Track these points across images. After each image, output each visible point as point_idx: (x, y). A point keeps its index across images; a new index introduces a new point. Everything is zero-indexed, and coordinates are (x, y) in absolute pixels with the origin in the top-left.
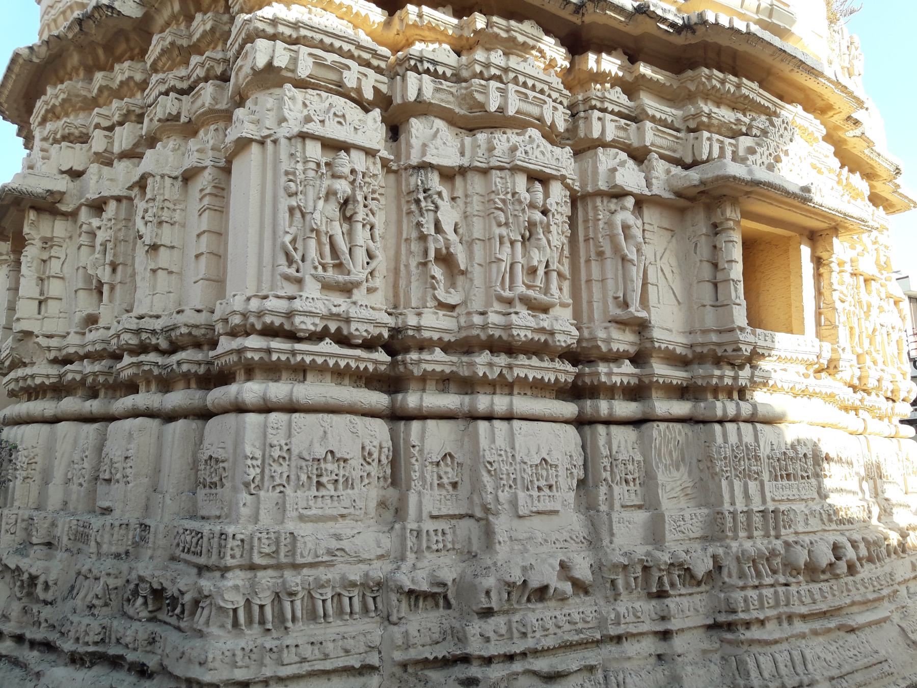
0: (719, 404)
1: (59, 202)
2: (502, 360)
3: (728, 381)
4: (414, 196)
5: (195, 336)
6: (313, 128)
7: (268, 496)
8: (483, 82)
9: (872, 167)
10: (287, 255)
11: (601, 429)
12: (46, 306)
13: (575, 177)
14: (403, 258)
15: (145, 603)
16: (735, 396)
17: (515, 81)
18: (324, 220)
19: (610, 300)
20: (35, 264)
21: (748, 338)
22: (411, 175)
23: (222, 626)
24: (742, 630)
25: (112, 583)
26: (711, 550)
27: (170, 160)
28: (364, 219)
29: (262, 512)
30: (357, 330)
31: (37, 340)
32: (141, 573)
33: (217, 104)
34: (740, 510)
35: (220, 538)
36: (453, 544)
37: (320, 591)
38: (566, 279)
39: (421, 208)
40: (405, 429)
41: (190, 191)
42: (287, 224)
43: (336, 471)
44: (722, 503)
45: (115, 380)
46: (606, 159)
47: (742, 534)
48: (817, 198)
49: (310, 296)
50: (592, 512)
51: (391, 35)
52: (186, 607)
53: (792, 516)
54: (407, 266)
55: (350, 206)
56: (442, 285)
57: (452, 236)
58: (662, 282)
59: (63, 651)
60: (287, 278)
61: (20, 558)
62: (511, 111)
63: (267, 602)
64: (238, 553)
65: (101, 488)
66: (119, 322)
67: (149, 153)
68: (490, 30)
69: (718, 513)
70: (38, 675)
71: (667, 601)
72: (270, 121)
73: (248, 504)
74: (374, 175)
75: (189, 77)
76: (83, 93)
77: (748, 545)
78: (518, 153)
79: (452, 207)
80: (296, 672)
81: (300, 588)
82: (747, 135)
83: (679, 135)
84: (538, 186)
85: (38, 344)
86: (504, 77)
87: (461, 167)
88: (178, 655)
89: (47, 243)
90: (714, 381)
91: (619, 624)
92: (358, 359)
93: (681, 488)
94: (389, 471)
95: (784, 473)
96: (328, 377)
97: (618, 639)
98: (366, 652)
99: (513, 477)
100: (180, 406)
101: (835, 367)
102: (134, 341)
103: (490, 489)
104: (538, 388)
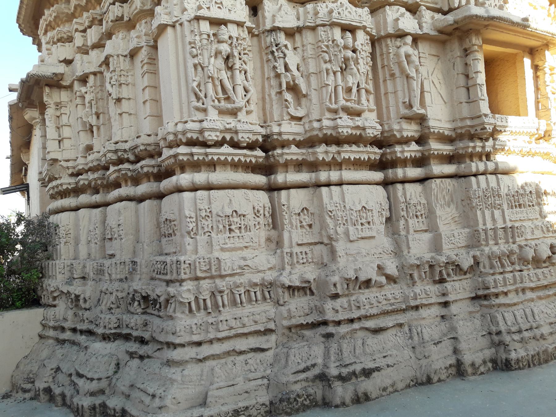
0: (473, 164)
1: (61, 80)
2: (333, 149)
3: (479, 149)
5: (149, 151)
6: (204, 12)
7: (202, 239)
10: (196, 94)
11: (399, 186)
12: (63, 143)
13: (372, 27)
14: (267, 90)
15: (139, 304)
16: (484, 158)
18: (216, 70)
19: (400, 105)
20: (53, 119)
21: (490, 121)
22: (267, 36)
23: (183, 312)
24: (493, 299)
25: (120, 295)
26: (472, 253)
27: (121, 45)
28: (240, 67)
29: (199, 248)
30: (242, 137)
31: (61, 163)
32: (135, 288)
33: (144, 6)
34: (489, 228)
35: (177, 264)
36: (312, 259)
37: (237, 289)
38: (371, 93)
39: (275, 57)
40: (278, 196)
41: (135, 63)
42: (194, 75)
43: (240, 222)
44: (478, 225)
47: (491, 242)
48: (533, 24)
49: (212, 119)
50: (396, 236)
52: (162, 304)
53: (523, 230)
54: (270, 95)
55: (231, 60)
56: (292, 105)
58: (433, 90)
59: (98, 334)
60: (197, 109)
61: (68, 286)
63: (208, 297)
64: (188, 271)
65: (108, 244)
66: (104, 148)
67: (108, 43)
69: (475, 231)
70: (86, 348)
72: (177, 12)
73: (191, 243)
74: (244, 39)
76: (66, 11)
77: (495, 248)
78: (334, 14)
79: (295, 54)
80: (228, 335)
81: (225, 288)
84: (348, 34)
87: (298, 27)
88: (160, 330)
89: (58, 106)
90: (470, 150)
91: (416, 299)
92: (245, 156)
93: (451, 218)
94: (270, 221)
95: (517, 204)
96: (229, 168)
97: (417, 308)
98: (267, 322)
100: (145, 192)
101: (549, 135)
102: (114, 157)
104: (358, 164)
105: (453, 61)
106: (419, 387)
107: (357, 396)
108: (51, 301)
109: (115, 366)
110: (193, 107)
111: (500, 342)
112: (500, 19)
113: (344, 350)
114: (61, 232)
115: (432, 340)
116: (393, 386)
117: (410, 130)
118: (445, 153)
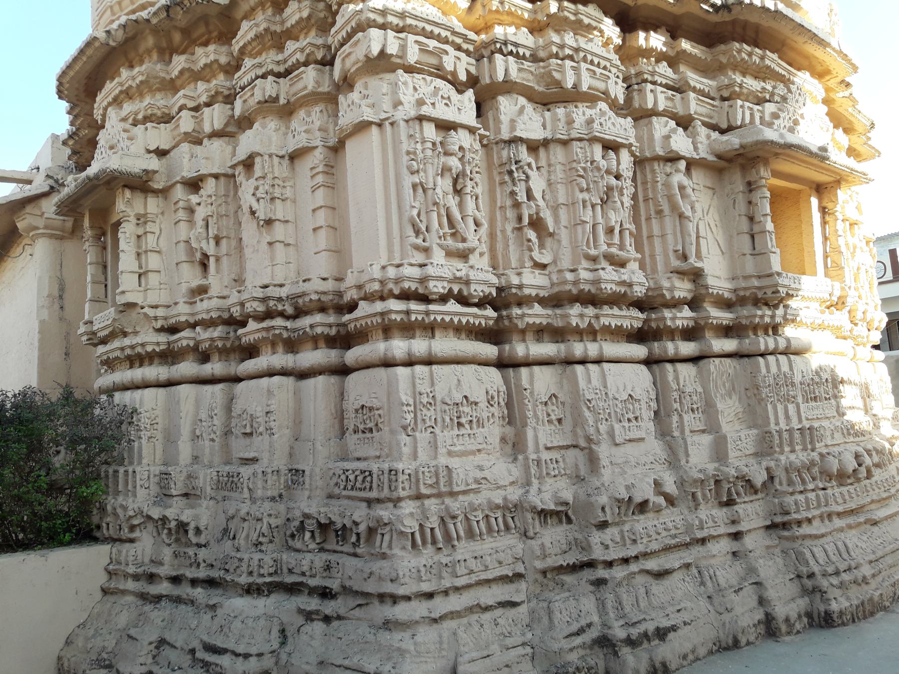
2: (590, 311)
3: (767, 320)
4: (507, 167)
7: (423, 437)
8: (559, 62)
9: (851, 123)
11: (669, 366)
14: (499, 224)
15: (313, 537)
17: (585, 59)
19: (671, 254)
22: (503, 149)
23: (404, 548)
25: (274, 522)
29: (419, 450)
30: (475, 290)
32: (307, 511)
44: (769, 423)
45: (232, 345)
46: (661, 127)
47: (787, 449)
50: (668, 438)
51: (473, 19)
54: (503, 231)
57: (541, 203)
60: (417, 248)
62: (584, 88)
64: (407, 485)
68: (561, 14)
71: (736, 507)
75: (285, 61)
76: (163, 75)
78: (595, 125)
82: (769, 101)
83: (715, 103)
84: (612, 154)
85: (145, 314)
86: (575, 57)
87: (545, 139)
89: (142, 219)
90: (757, 320)
91: (702, 529)
92: (476, 316)
94: (506, 412)
97: (703, 541)
99: (608, 411)
101: (843, 303)
102: (261, 308)
103: (591, 423)
105: (733, 196)
106: (725, 653)
107: (654, 666)
108: (125, 533)
109: (278, 634)
110: (411, 245)
111: (814, 588)
112: (790, 146)
113: (625, 603)
114: (143, 420)
115: (731, 587)
116: (693, 652)
117: (683, 289)
118: (724, 323)
